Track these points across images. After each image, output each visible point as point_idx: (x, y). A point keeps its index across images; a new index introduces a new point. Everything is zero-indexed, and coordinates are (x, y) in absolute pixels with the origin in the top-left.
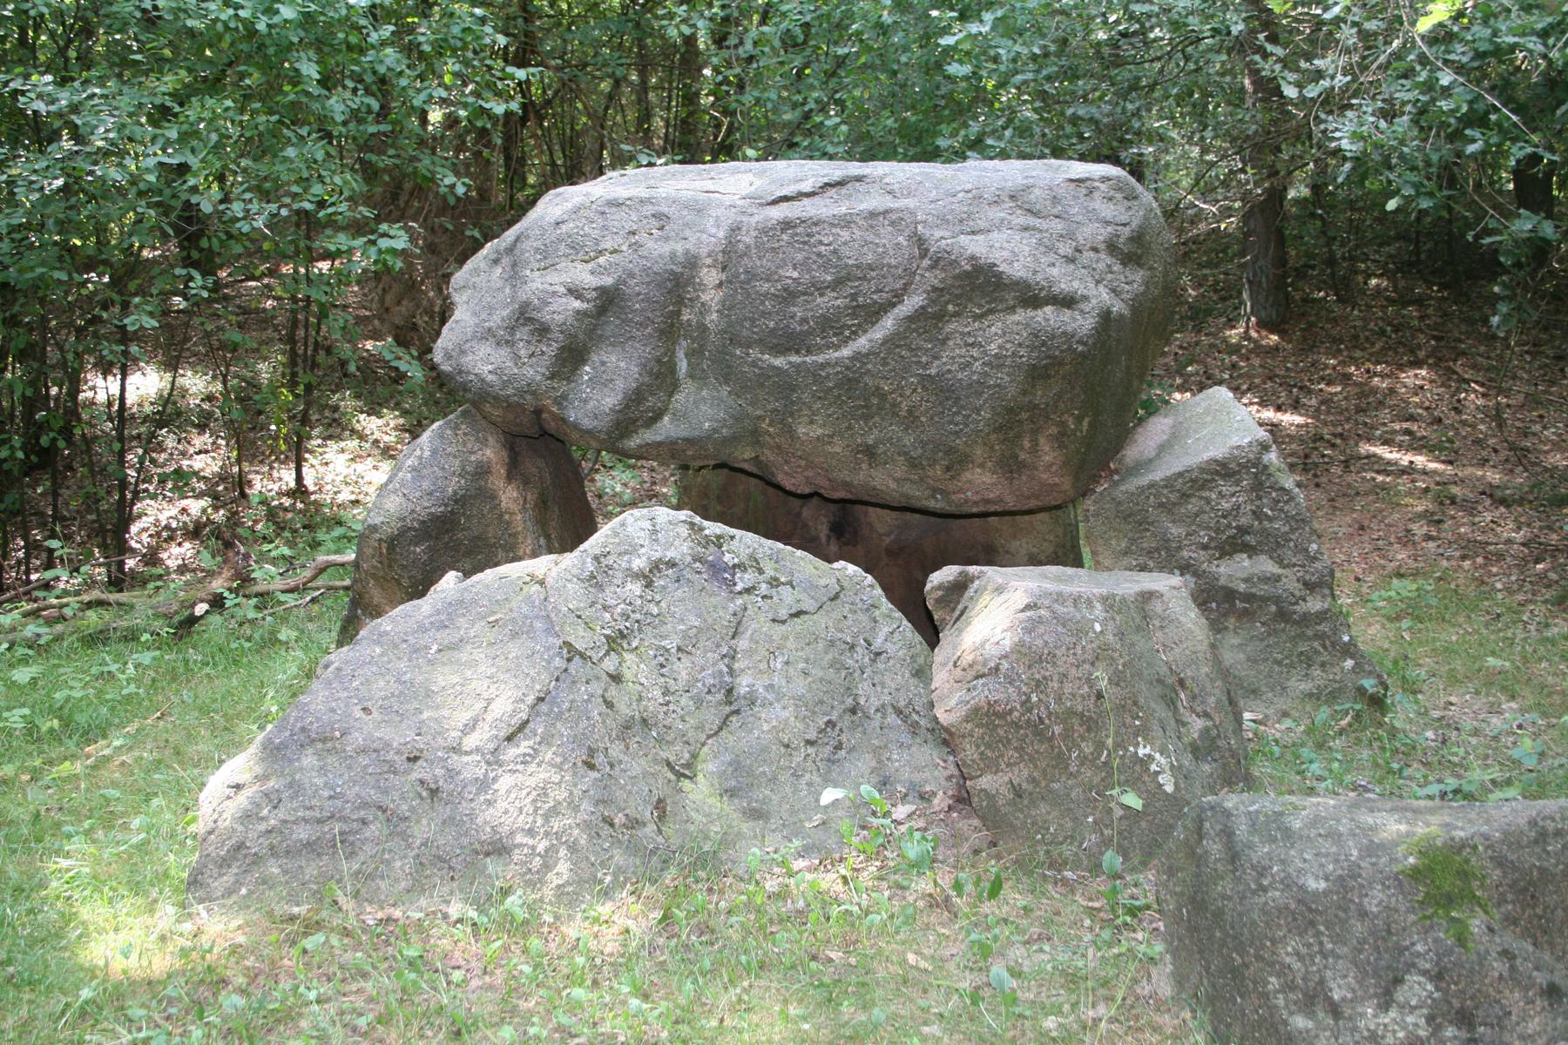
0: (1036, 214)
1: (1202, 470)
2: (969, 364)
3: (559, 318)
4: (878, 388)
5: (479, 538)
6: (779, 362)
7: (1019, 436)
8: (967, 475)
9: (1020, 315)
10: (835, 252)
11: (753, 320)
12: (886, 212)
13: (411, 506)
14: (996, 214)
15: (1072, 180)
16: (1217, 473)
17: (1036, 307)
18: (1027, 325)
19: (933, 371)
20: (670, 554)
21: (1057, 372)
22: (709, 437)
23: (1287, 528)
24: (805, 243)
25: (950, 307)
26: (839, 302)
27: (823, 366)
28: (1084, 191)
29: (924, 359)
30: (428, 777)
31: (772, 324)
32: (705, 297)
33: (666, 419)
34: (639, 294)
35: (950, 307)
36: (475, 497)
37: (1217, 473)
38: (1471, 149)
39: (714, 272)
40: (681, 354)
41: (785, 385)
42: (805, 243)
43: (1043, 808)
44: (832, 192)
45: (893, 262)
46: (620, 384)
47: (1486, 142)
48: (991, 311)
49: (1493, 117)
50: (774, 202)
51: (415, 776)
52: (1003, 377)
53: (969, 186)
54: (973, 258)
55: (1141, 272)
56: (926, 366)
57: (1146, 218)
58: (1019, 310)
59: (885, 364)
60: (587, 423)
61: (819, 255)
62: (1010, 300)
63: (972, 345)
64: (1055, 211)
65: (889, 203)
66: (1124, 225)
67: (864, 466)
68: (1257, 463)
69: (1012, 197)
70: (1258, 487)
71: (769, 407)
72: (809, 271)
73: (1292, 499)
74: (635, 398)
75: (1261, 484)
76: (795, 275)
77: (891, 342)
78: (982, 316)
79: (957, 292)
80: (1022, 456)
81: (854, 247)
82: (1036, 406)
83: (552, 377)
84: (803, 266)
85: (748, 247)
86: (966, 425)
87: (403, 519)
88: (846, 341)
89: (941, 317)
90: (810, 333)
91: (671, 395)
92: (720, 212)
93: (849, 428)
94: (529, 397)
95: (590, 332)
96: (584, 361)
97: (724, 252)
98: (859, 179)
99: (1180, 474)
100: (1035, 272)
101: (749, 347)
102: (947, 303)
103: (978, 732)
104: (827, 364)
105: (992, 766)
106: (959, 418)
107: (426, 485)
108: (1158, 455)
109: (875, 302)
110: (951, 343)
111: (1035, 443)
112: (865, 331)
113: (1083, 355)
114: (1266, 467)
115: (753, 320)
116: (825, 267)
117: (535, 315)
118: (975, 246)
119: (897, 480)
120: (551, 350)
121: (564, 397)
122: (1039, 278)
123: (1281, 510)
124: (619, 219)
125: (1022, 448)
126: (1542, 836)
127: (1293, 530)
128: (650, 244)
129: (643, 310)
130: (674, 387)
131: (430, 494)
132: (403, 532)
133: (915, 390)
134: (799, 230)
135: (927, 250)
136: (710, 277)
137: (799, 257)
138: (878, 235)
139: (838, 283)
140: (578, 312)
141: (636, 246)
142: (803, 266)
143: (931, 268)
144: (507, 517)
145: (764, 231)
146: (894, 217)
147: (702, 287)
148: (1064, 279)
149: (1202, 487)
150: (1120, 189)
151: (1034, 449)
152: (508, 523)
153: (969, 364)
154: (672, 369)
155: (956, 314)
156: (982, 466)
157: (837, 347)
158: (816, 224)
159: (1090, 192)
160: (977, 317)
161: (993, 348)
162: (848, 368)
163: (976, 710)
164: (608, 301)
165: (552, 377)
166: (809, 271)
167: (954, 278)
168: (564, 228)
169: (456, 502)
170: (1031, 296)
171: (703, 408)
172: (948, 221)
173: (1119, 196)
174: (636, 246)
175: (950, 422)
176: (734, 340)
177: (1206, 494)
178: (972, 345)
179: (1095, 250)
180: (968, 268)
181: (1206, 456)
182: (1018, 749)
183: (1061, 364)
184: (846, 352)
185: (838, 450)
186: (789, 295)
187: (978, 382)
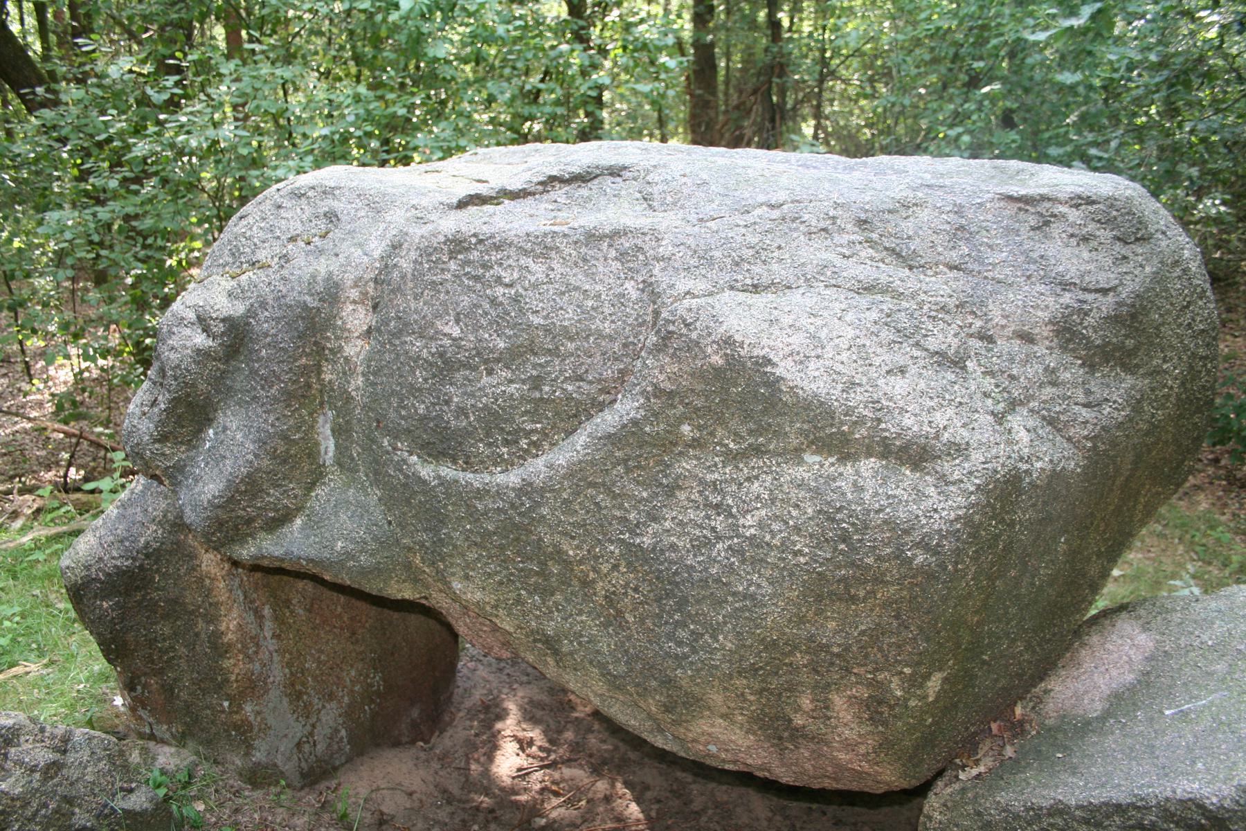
2: (708, 544)
4: (560, 552)
5: (175, 602)
6: (426, 471)
10: (516, 300)
12: (616, 234)
13: (100, 552)
14: (814, 253)
15: (1010, 198)
17: (844, 458)
19: (647, 541)
21: (873, 593)
22: (341, 563)
24: (477, 279)
25: (686, 429)
26: (512, 388)
27: (481, 493)
28: (1033, 221)
29: (632, 516)
31: (422, 409)
32: (349, 350)
33: (298, 522)
34: (266, 335)
35: (686, 429)
36: (170, 553)
39: (361, 311)
42: (477, 279)
45: (607, 328)
48: (758, 451)
50: (462, 204)
53: (781, 196)
54: (728, 341)
55: (1129, 380)
56: (634, 529)
57: (1158, 278)
58: (810, 458)
61: (493, 302)
62: (793, 431)
64: (954, 256)
66: (1104, 292)
69: (862, 223)
76: (456, 332)
77: (577, 474)
78: (742, 455)
79: (699, 403)
83: (163, 439)
87: (88, 568)
88: (524, 455)
89: (669, 444)
91: (312, 486)
96: (209, 421)
97: (376, 281)
98: (615, 172)
99: (1119, 808)
100: (852, 385)
101: (396, 438)
102: (680, 421)
106: (682, 634)
108: (1106, 715)
109: (569, 398)
110: (682, 495)
116: (497, 326)
122: (857, 398)
125: (798, 709)
129: (269, 359)
133: (615, 567)
134: (474, 255)
136: (356, 318)
137: (466, 301)
138: (591, 276)
139: (512, 357)
140: (198, 351)
144: (207, 582)
145: (427, 252)
146: (626, 243)
147: (344, 334)
150: (1108, 222)
153: (708, 544)
154: (312, 452)
155: (696, 443)
157: (508, 465)
158: (497, 248)
159: (1045, 223)
160: (732, 457)
165: (163, 439)
166: (477, 328)
167: (693, 375)
169: (147, 556)
172: (711, 262)
173: (1105, 234)
175: (671, 637)
179: (1027, 338)
180: (717, 360)
181: (1187, 786)
183: (879, 580)
184: (513, 478)
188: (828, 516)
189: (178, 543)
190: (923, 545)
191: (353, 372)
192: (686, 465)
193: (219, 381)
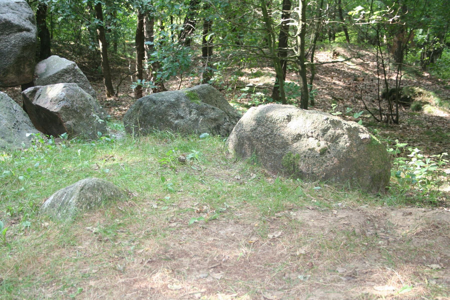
0: (13, 10)
1: (61, 72)
2: (7, 47)
7: (21, 65)
8: (9, 76)
9: (18, 34)
15: (16, 2)
16: (65, 72)
18: (20, 36)
23: (83, 84)
37: (65, 72)
43: (79, 128)
48: (11, 33)
54: (5, 19)
62: (15, 29)
63: (7, 42)
68: (74, 69)
70: (74, 75)
73: (83, 77)
75: (75, 74)
80: (22, 70)
82: (24, 57)
86: (8, 62)
99: (57, 73)
103: (64, 112)
105: (68, 119)
106: (6, 61)
111: (24, 66)
113: (34, 43)
114: (76, 70)
126: (203, 89)
127: (85, 84)
148: (28, 25)
149: (62, 76)
151: (24, 68)
156: (12, 73)
159: (21, 5)
160: (7, 35)
161: (13, 42)
163: (63, 107)
170: (20, 29)
175: (4, 62)
177: (63, 78)
178: (7, 42)
187: (10, 51)
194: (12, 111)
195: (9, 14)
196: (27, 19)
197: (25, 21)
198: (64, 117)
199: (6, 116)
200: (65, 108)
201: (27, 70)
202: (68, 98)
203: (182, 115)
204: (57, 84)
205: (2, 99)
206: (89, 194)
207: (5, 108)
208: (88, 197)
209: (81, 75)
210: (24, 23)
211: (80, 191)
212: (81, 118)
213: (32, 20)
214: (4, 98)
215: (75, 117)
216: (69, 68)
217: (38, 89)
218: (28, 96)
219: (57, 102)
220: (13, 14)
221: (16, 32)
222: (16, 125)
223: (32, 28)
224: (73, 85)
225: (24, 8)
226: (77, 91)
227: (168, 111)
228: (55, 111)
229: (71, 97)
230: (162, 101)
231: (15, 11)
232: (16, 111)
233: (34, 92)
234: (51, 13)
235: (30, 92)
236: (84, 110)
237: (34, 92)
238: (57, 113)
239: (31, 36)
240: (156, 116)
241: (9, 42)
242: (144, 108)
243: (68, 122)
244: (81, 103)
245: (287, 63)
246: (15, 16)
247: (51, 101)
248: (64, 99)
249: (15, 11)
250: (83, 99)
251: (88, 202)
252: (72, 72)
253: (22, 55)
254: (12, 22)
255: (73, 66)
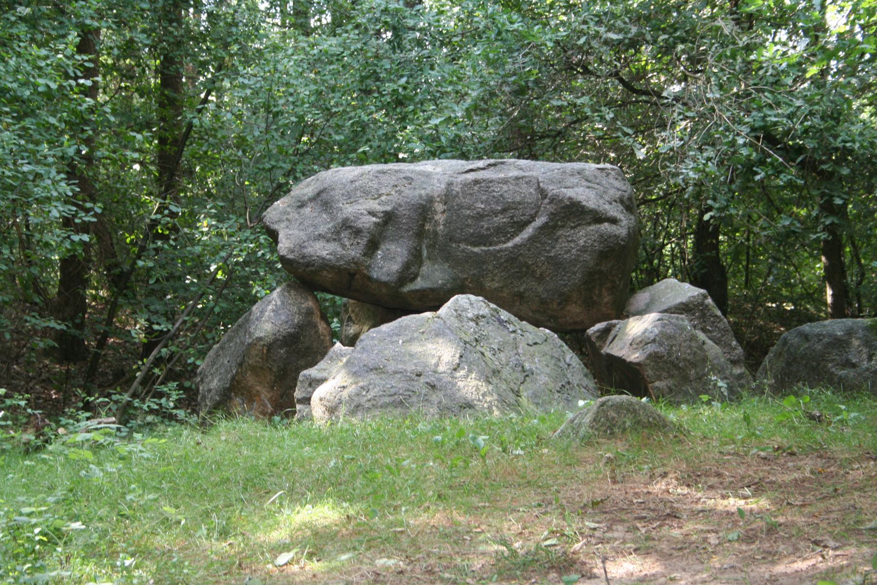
0: (590, 182)
2: (569, 251)
3: (367, 225)
6: (476, 250)
8: (569, 308)
9: (592, 227)
10: (501, 195)
11: (462, 229)
13: (277, 328)
18: (597, 232)
19: (552, 254)
20: (481, 313)
22: (441, 288)
23: (720, 335)
30: (428, 380)
31: (472, 231)
32: (437, 217)
33: (419, 279)
35: (559, 223)
37: (684, 310)
38: (757, 178)
39: (441, 205)
40: (424, 247)
41: (479, 261)
44: (492, 168)
45: (529, 201)
46: (399, 259)
47: (766, 173)
48: (579, 225)
49: (769, 160)
50: (467, 172)
51: (422, 381)
52: (586, 257)
54: (570, 198)
56: (549, 252)
59: (529, 250)
60: (384, 278)
61: (494, 197)
62: (588, 218)
63: (571, 241)
65: (520, 173)
67: (517, 304)
68: (702, 304)
70: (703, 316)
71: (471, 273)
72: (490, 204)
73: (721, 320)
74: (407, 266)
76: (483, 206)
77: (532, 239)
79: (563, 215)
80: (595, 298)
81: (510, 193)
83: (365, 255)
84: (486, 202)
85: (458, 193)
87: (275, 335)
88: (508, 240)
89: (555, 227)
90: (490, 235)
91: (420, 267)
92: (439, 176)
93: (512, 283)
94: (353, 265)
95: (380, 234)
101: (460, 242)
103: (652, 364)
104: (501, 250)
105: (659, 378)
106: (565, 278)
107: (283, 317)
112: (517, 235)
113: (624, 247)
114: (707, 306)
115: (462, 229)
116: (497, 203)
117: (352, 224)
118: (570, 193)
119: (533, 312)
120: (363, 241)
121: (370, 266)
123: (716, 327)
124: (384, 179)
127: (723, 336)
128: (407, 191)
129: (407, 223)
130: (420, 264)
131: (287, 322)
132: (276, 341)
134: (483, 185)
135: (546, 195)
136: (439, 207)
137: (484, 197)
139: (504, 211)
140: (375, 223)
141: (400, 192)
142: (486, 202)
143: (550, 203)
145: (465, 185)
146: (527, 180)
147: (435, 212)
148: (614, 211)
151: (600, 295)
152: (323, 341)
153: (569, 251)
155: (563, 226)
156: (575, 303)
157: (505, 243)
158: (491, 182)
159: (608, 175)
160: (572, 228)
161: (581, 242)
162: (511, 252)
163: (650, 355)
164: (389, 218)
166: (490, 204)
168: (357, 184)
169: (299, 327)
170: (598, 218)
171: (437, 274)
174: (400, 192)
175: (561, 280)
176: (452, 239)
178: (571, 241)
180: (568, 203)
182: (668, 372)
184: (510, 244)
185: (505, 295)
186: (480, 216)
187: (575, 260)
188: (601, 236)
189: (309, 321)
190: (622, 240)
191: (439, 225)
192: (560, 232)
193: (380, 234)
194: (562, 364)
195: (580, 190)
196: (615, 201)
197: (610, 203)
198: (650, 372)
199: (548, 370)
200: (654, 357)
201: (606, 300)
202: (662, 338)
203: (854, 361)
204: (647, 316)
205: (546, 341)
206: (612, 414)
207: (548, 357)
208: (610, 417)
209: (716, 316)
210: (607, 207)
211: (599, 408)
212: (686, 379)
213: (627, 203)
214: (549, 341)
215: (672, 376)
216: (691, 302)
217: (614, 325)
218: (593, 339)
219: (641, 345)
220: (587, 190)
221: (589, 224)
222: (565, 388)
223: (623, 218)
224: (677, 319)
225: (612, 181)
226: (683, 329)
227: (828, 353)
228: (635, 361)
229: (670, 337)
230: (820, 335)
231: (593, 185)
232: (569, 365)
233: (607, 331)
234: (687, 200)
235: (598, 331)
236: (694, 365)
237: (607, 331)
238: (638, 364)
239: (617, 233)
240: (807, 363)
241: (575, 241)
242: (788, 350)
243: (657, 384)
244: (689, 351)
245: (686, 160)
246: (592, 194)
247: (631, 344)
248: (654, 341)
249: (593, 185)
250: (694, 344)
251: (608, 424)
252: (699, 310)
253: (598, 268)
254: (584, 203)
255: (701, 297)
